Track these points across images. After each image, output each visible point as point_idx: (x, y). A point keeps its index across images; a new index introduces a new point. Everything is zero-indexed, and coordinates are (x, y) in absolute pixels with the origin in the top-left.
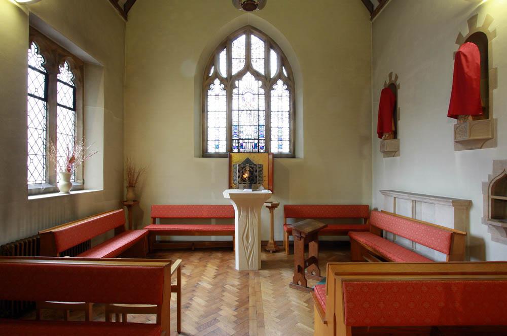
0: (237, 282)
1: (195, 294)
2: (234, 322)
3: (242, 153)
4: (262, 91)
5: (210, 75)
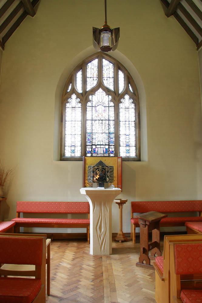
0: (92, 263)
1: (58, 271)
2: (92, 289)
3: (94, 156)
4: (112, 104)
5: (69, 91)
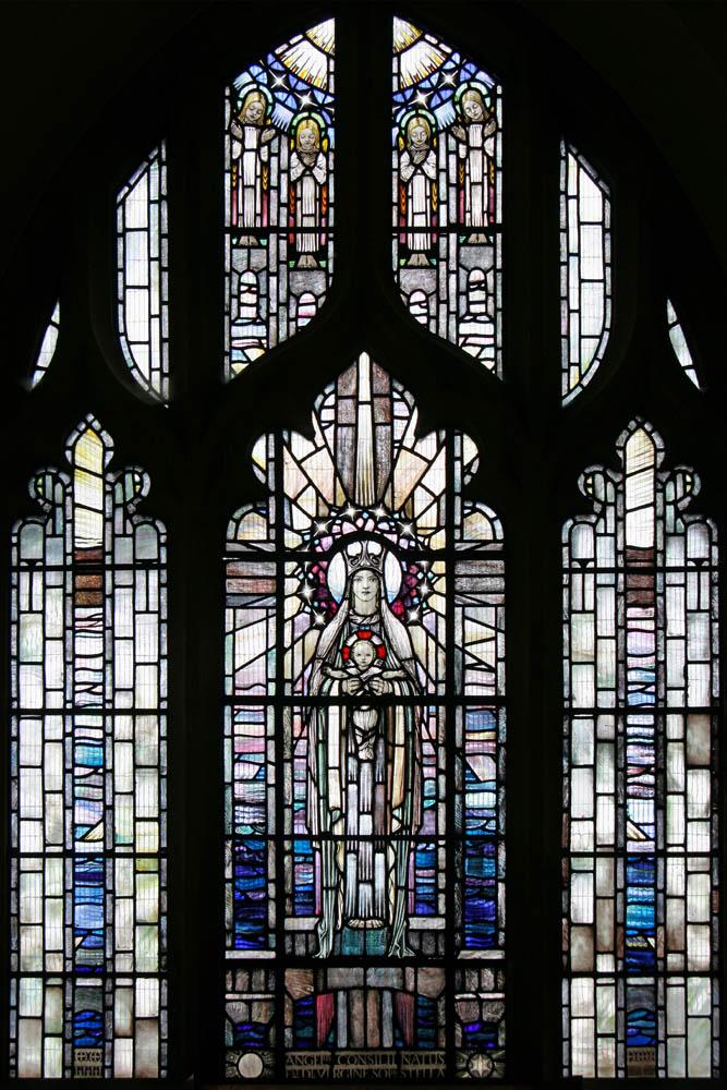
5: (572, 383)
